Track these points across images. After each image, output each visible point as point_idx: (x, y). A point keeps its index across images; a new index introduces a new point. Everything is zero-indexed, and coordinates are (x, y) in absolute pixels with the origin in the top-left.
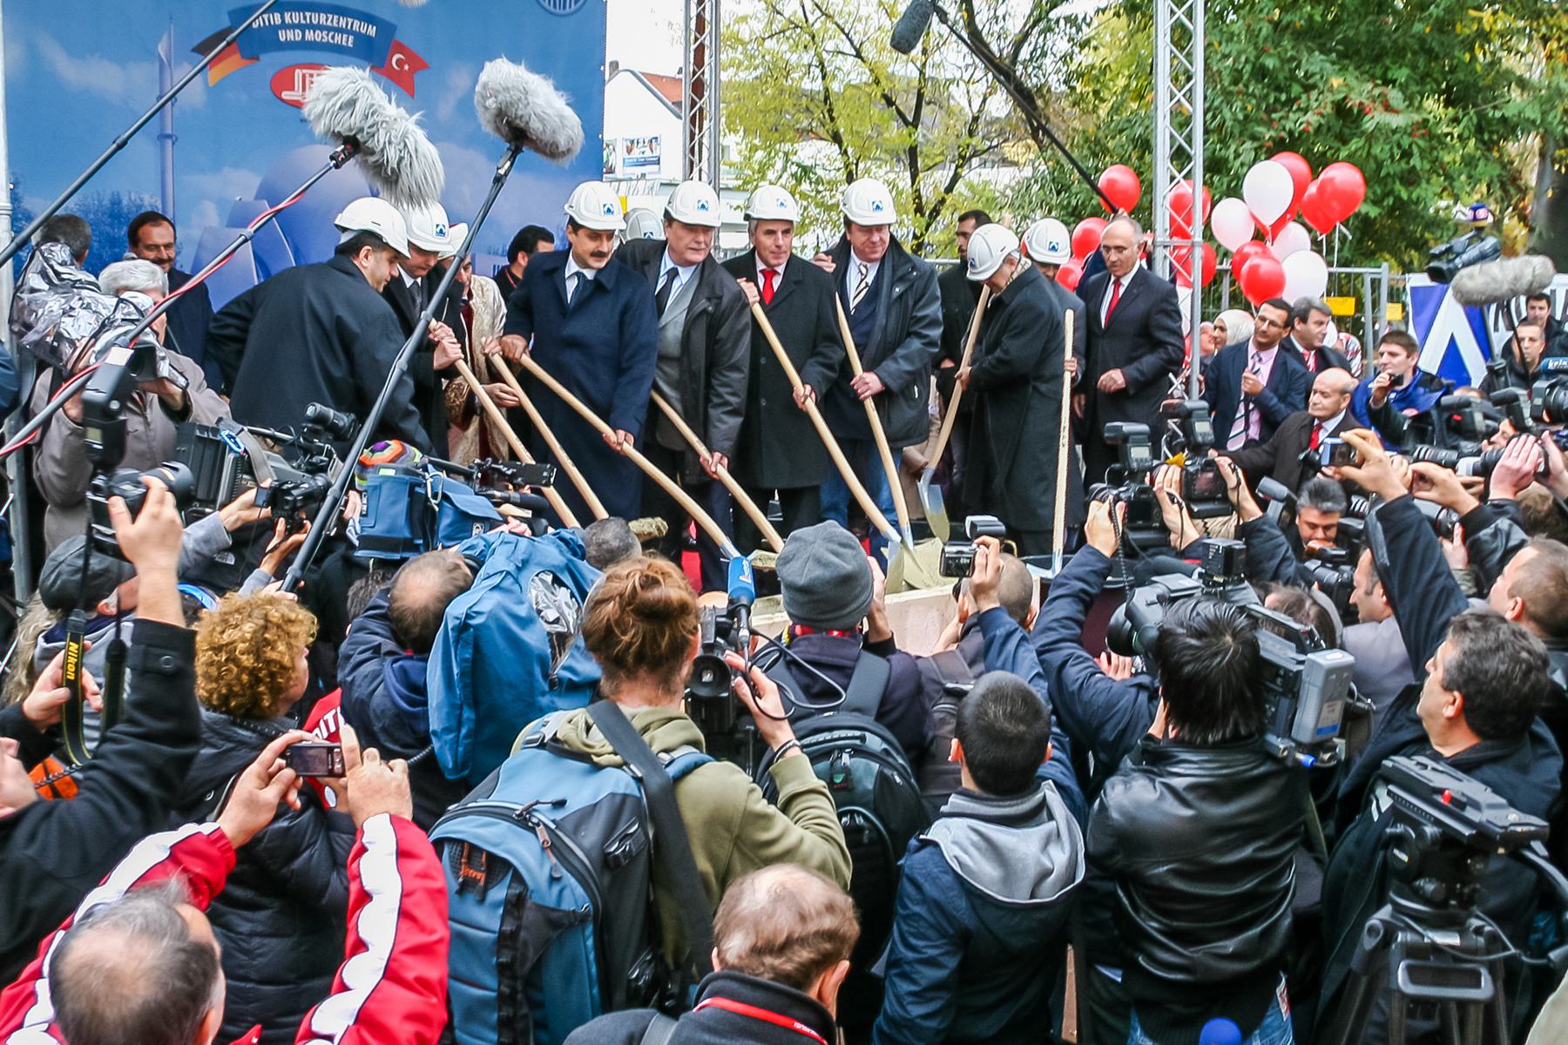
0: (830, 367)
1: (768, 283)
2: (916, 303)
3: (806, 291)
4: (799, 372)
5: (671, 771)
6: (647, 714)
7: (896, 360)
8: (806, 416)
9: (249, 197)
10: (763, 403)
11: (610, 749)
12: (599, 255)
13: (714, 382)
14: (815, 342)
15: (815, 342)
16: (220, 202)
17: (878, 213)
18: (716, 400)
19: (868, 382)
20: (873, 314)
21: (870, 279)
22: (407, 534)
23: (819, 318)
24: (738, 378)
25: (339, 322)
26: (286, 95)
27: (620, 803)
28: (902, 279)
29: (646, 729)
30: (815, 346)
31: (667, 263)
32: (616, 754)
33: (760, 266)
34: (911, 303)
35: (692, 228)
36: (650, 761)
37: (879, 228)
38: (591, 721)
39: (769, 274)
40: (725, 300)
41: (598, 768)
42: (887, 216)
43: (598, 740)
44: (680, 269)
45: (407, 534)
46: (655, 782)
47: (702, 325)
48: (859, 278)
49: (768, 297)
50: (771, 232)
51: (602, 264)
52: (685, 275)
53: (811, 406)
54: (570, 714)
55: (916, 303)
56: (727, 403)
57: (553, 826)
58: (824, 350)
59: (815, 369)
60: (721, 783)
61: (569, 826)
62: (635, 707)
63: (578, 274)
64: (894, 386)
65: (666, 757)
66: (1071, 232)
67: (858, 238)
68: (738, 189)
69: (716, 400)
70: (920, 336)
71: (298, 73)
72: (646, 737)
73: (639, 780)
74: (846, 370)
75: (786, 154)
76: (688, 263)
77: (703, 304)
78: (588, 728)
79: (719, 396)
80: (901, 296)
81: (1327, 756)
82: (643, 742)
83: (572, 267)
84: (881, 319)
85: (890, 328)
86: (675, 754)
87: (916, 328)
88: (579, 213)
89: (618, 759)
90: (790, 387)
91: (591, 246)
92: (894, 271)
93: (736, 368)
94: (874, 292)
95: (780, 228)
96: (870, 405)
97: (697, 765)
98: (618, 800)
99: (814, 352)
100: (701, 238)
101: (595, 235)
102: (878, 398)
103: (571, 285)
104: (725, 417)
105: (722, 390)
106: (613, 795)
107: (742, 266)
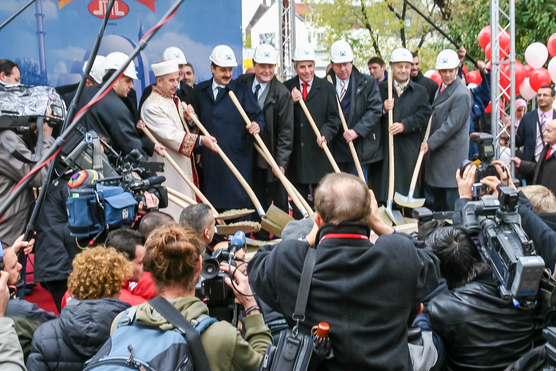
0: (334, 127)
1: (305, 90)
2: (368, 95)
3: (321, 91)
4: (319, 130)
5: (199, 329)
6: (181, 301)
7: (362, 122)
8: (322, 150)
9: (81, 59)
10: (302, 144)
11: (165, 321)
12: (226, 78)
13: (279, 135)
14: (327, 116)
15: (327, 116)
16: (67, 62)
17: (343, 57)
18: (280, 143)
19: (350, 134)
20: (349, 103)
21: (346, 88)
22: (90, 223)
23: (328, 105)
24: (289, 132)
25: (99, 115)
27: (178, 348)
28: (360, 85)
29: (182, 309)
30: (327, 118)
31: (256, 82)
32: (168, 323)
33: (301, 82)
34: (366, 96)
35: (263, 65)
36: (188, 325)
37: (345, 64)
38: (152, 308)
39: (306, 85)
40: (280, 98)
41: (162, 332)
42: (349, 57)
43: (158, 318)
44: (261, 85)
45: (90, 223)
46: (191, 335)
47: (271, 109)
48: (342, 87)
49: (305, 96)
50: (303, 67)
51: (228, 82)
52: (263, 87)
53: (325, 146)
54: (141, 306)
55: (368, 95)
56: (284, 144)
57: (148, 366)
58: (331, 120)
59: (326, 128)
60: (223, 332)
61: (155, 364)
62: (171, 297)
63: (218, 88)
64: (363, 134)
65: (195, 322)
66: (57, 6)
67: (336, 69)
68: (325, 52)
69: (280, 143)
70: (372, 109)
72: (183, 313)
73: (184, 335)
74: (342, 130)
75: (346, 35)
76: (264, 82)
77: (271, 99)
78: (152, 312)
79: (281, 141)
80: (361, 93)
81: (206, 299)
82: (181, 315)
83: (215, 85)
84: (353, 105)
85: (358, 108)
86: (199, 320)
87: (371, 106)
88: (216, 60)
89: (170, 326)
90: (315, 137)
91: (222, 74)
92: (356, 82)
93: (288, 127)
94: (348, 93)
95: (306, 64)
96: (351, 145)
97: (211, 324)
98: (177, 347)
99: (326, 120)
100: (268, 70)
101: (224, 69)
102: (355, 141)
103: (216, 93)
104: (283, 151)
105: (282, 139)
106: (174, 345)
107: (293, 83)
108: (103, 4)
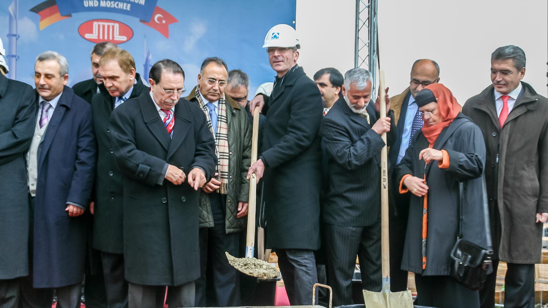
26: (87, 36)
71: (95, 24)
108: (99, 26)
